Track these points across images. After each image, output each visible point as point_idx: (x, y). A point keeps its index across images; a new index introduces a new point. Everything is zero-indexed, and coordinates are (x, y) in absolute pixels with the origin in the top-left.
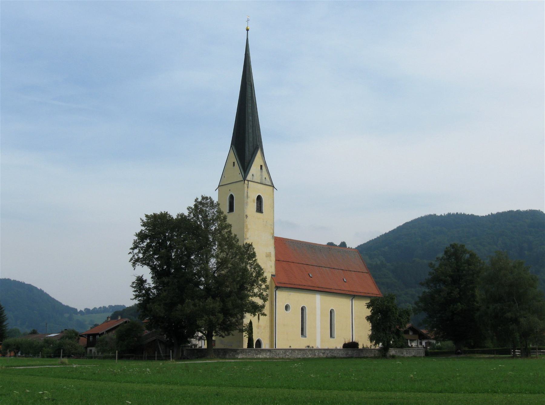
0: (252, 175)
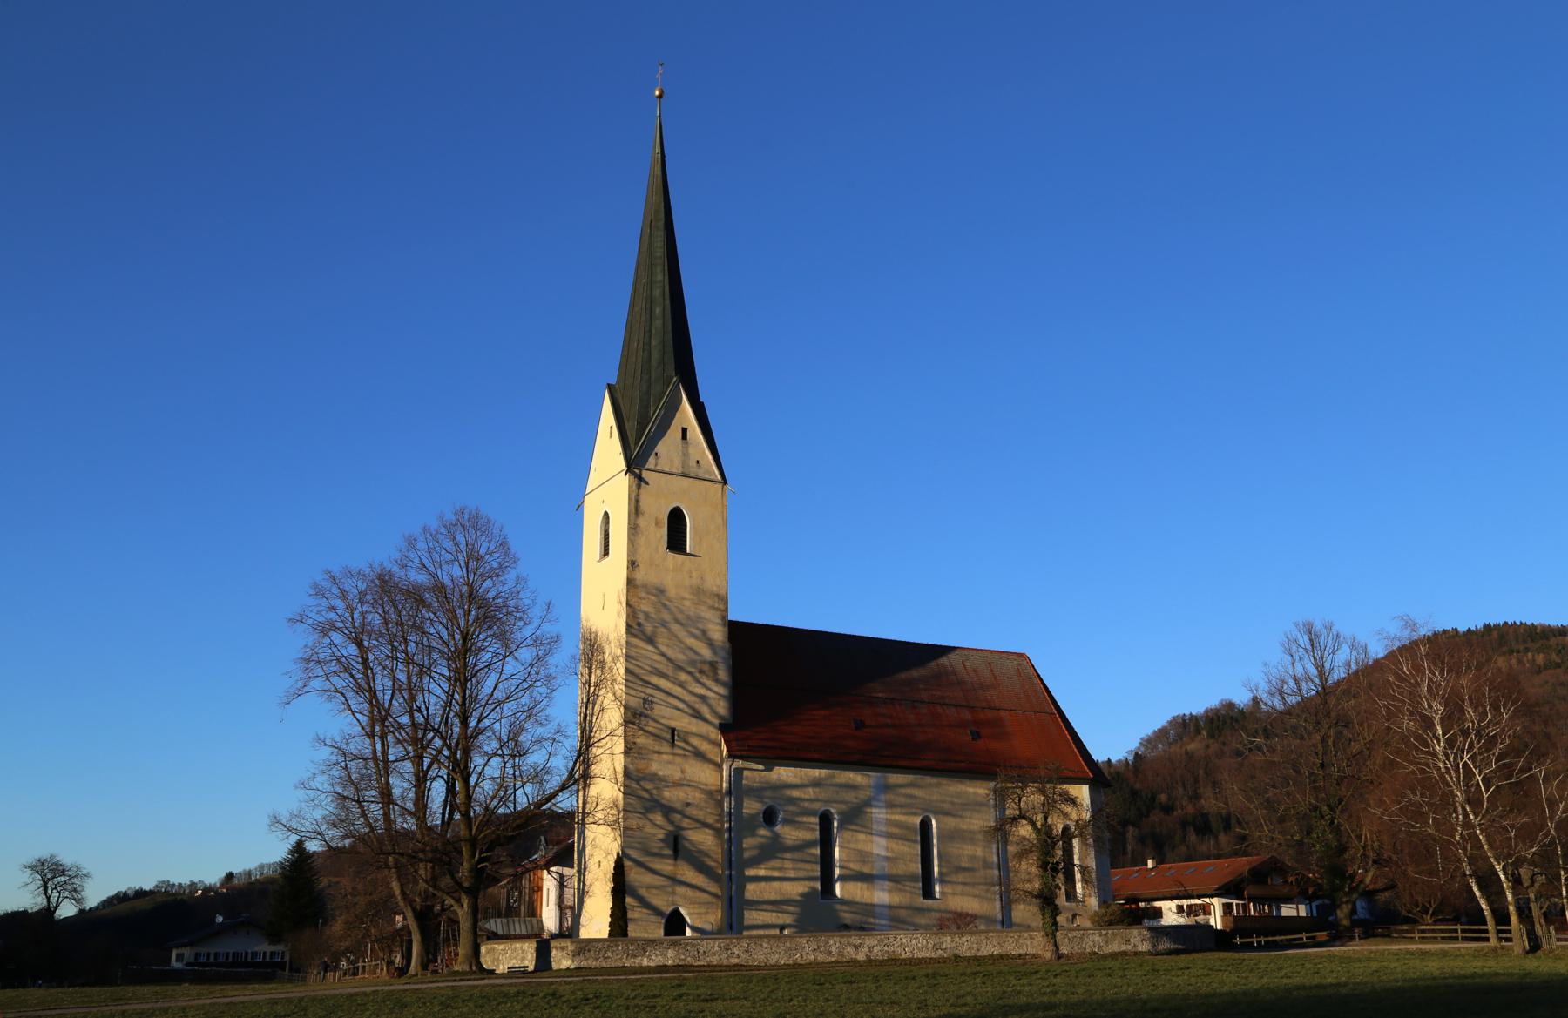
0: (695, 464)
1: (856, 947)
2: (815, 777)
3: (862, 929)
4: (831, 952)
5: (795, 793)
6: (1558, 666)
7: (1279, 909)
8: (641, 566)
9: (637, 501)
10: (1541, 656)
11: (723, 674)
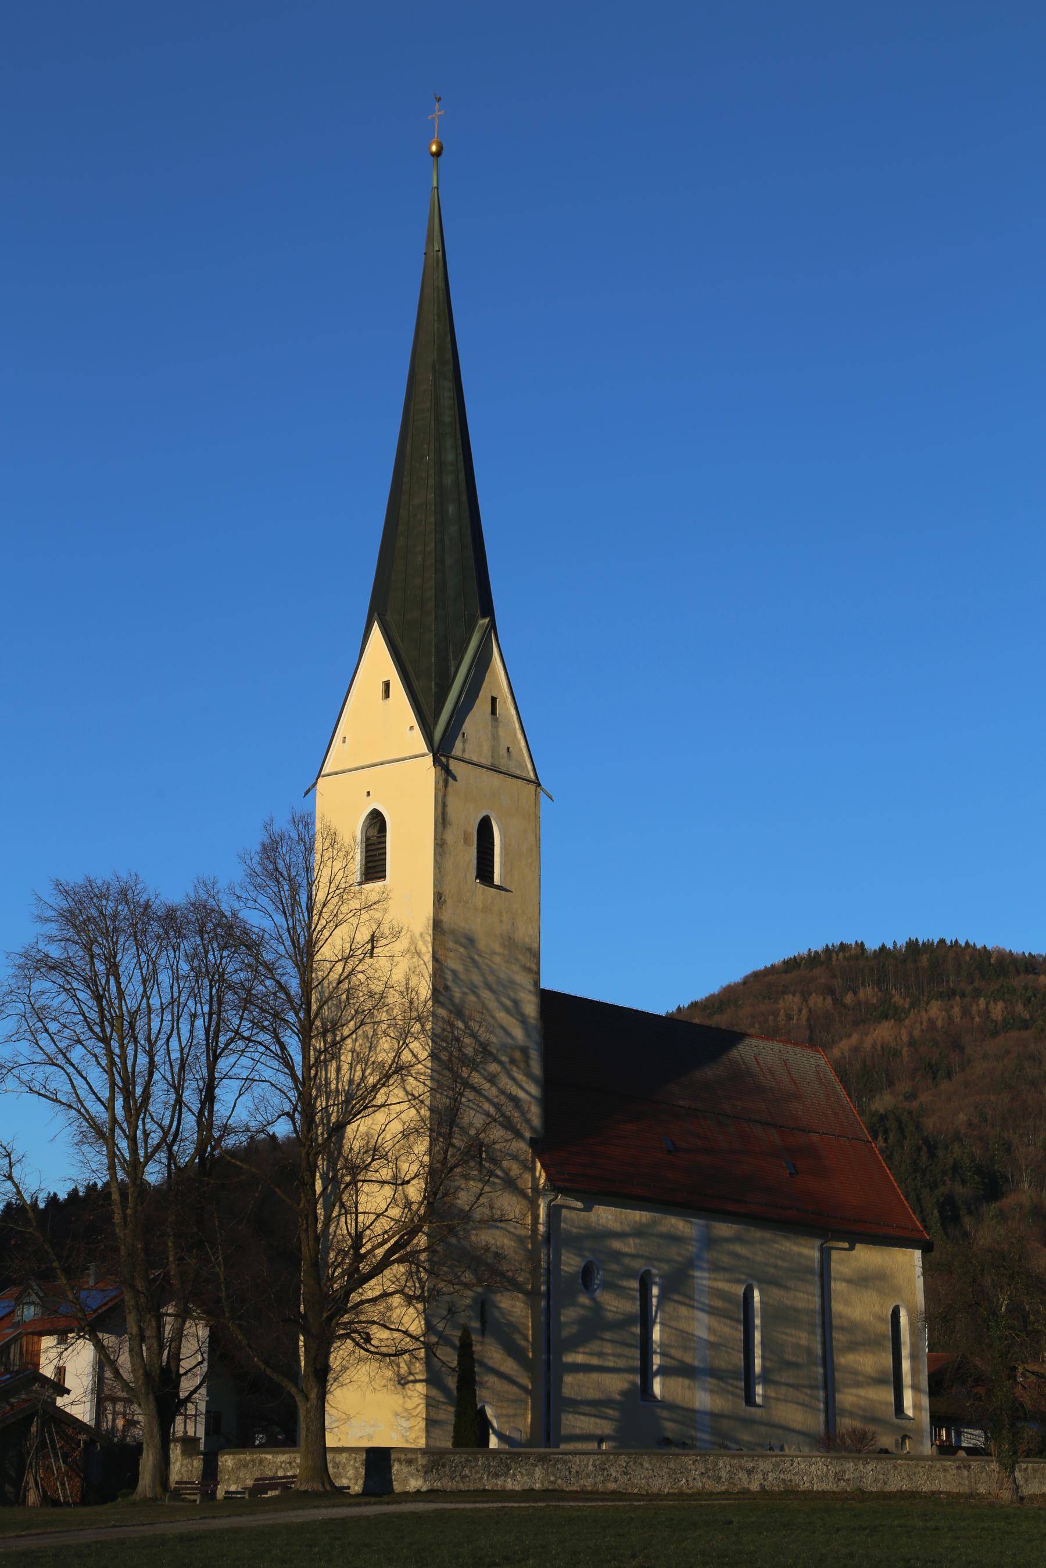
1: (750, 1472)
2: (636, 1222)
3: (684, 1445)
4: (720, 1478)
5: (617, 1245)
6: (1025, 1025)
7: (959, 1435)
8: (449, 902)
9: (444, 805)
10: (1000, 1005)
11: (536, 1068)
